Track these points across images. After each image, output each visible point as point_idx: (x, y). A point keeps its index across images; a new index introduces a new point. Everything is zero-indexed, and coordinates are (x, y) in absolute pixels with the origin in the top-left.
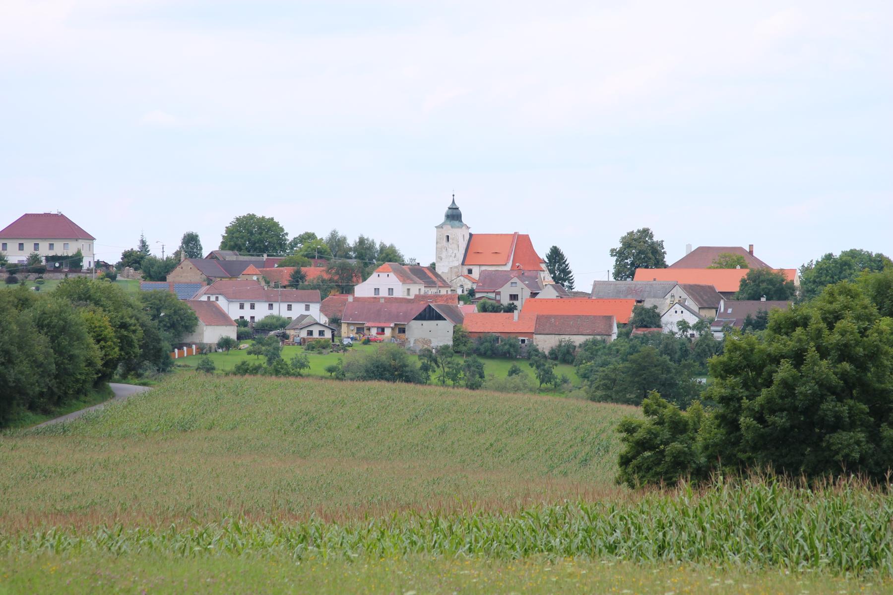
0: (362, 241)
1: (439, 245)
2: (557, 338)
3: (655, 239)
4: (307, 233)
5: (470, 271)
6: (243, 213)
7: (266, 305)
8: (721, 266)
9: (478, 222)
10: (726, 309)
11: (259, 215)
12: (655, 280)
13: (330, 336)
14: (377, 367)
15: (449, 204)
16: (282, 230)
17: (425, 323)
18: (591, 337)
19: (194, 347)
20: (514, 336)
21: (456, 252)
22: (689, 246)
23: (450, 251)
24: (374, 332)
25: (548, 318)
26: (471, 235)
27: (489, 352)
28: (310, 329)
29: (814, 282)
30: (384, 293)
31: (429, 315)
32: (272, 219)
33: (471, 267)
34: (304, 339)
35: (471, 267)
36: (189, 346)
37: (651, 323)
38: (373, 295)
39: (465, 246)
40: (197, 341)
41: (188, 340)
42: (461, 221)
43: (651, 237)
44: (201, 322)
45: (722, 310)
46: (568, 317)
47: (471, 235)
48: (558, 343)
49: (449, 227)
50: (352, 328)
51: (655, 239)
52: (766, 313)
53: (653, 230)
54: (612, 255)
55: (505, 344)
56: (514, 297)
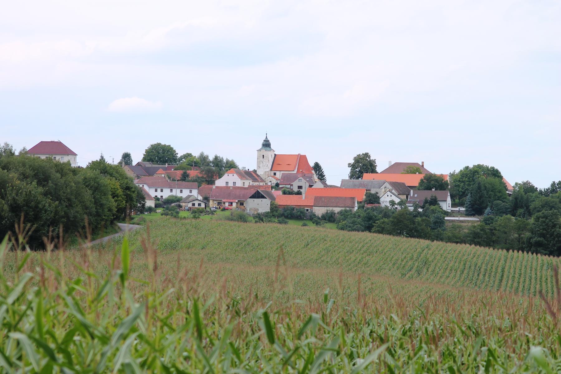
2: (326, 208)
3: (371, 158)
5: (275, 174)
6: (155, 142)
7: (169, 190)
9: (279, 148)
10: (414, 195)
11: (163, 143)
13: (204, 206)
15: (264, 138)
16: (175, 151)
17: (255, 200)
18: (344, 208)
22: (390, 162)
23: (265, 163)
24: (227, 204)
25: (321, 198)
26: (275, 155)
28: (193, 202)
29: (459, 181)
31: (257, 195)
38: (225, 185)
39: (272, 161)
43: (369, 157)
50: (215, 202)
51: (371, 158)
52: (435, 197)
56: (300, 187)
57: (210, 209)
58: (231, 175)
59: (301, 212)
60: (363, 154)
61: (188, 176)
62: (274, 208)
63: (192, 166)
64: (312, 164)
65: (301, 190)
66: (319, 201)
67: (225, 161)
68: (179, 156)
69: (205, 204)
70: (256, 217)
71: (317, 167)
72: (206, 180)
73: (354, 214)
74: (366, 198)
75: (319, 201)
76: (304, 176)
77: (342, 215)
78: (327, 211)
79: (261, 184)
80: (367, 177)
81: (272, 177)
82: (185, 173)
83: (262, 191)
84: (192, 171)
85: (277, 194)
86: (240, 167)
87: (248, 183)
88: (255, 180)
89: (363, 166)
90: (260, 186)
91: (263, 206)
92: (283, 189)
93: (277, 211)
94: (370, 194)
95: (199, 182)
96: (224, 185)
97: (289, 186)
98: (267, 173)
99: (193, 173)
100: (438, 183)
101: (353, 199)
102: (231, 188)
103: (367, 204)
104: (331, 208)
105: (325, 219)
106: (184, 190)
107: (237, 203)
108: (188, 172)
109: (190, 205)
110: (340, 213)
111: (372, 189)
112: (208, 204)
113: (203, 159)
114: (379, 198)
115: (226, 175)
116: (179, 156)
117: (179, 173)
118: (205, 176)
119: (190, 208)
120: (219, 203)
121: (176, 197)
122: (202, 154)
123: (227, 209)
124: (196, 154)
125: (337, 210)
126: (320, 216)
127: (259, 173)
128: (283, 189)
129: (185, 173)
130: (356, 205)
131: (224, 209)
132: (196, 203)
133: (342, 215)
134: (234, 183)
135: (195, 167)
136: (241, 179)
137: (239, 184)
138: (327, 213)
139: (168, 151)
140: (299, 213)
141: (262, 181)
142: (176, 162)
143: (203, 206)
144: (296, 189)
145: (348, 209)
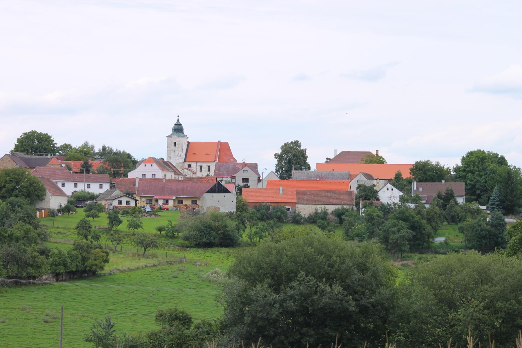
0: (104, 148)
1: (169, 149)
2: (314, 206)
3: (302, 148)
4: (65, 144)
5: (189, 166)
6: (28, 130)
7: (73, 184)
8: (367, 162)
9: (193, 134)
10: (417, 188)
11: (39, 131)
12: (333, 170)
13: (134, 205)
14: (206, 227)
15: (175, 122)
16: (53, 141)
17: (215, 195)
18: (340, 207)
19: (43, 211)
20: (282, 205)
21: (181, 153)
22: (336, 151)
23: (177, 152)
24: (160, 202)
25: (305, 192)
26: (189, 143)
27: (265, 217)
28: (120, 199)
29: (464, 171)
30: (149, 176)
31: (218, 189)
32: (47, 134)
33: (190, 163)
34: (116, 207)
35: (190, 163)
36: (40, 210)
37: (373, 197)
38: (151, 178)
39: (185, 149)
40: (46, 207)
41: (38, 206)
42: (183, 133)
43: (300, 146)
44: (48, 193)
45: (415, 189)
46: (320, 191)
47: (189, 143)
48: (314, 211)
49: (176, 137)
50: (144, 199)
51: (302, 148)
52: (452, 191)
53: (301, 141)
54: (275, 158)
55: (277, 211)
56: (245, 180)
60: (292, 142)
75: (303, 197)
89: (292, 159)
100: (437, 173)
104: (323, 207)
139: (46, 140)
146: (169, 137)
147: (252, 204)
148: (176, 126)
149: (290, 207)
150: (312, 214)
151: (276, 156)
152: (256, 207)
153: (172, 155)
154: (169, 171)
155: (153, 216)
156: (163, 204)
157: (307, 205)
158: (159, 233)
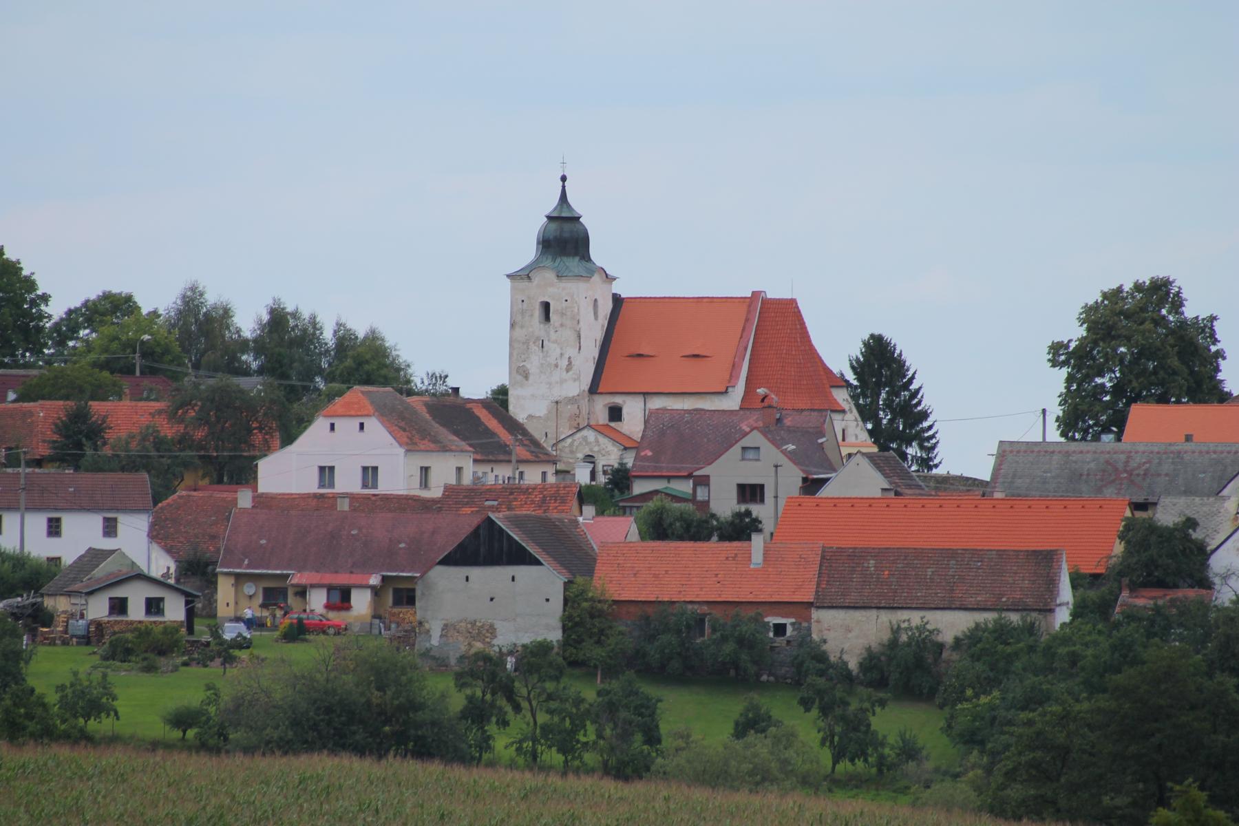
1: (519, 332)
2: (886, 617)
3: (1189, 312)
4: (107, 296)
5: (615, 413)
9: (641, 259)
12: (1188, 438)
14: (329, 710)
15: (550, 204)
16: (30, 284)
17: (476, 572)
18: (990, 616)
21: (571, 352)
23: (553, 350)
24: (317, 601)
25: (856, 556)
26: (617, 300)
28: (119, 593)
30: (348, 482)
31: (487, 547)
33: (618, 400)
35: (618, 400)
39: (599, 334)
43: (1178, 304)
46: (920, 553)
48: (886, 636)
49: (550, 275)
50: (249, 589)
51: (1189, 312)
54: (1055, 363)
55: (724, 639)
56: (750, 493)
57: (215, 632)
58: (347, 426)
59: (741, 642)
60: (1138, 287)
61: (95, 433)
62: (584, 618)
63: (128, 370)
64: (839, 352)
65: (756, 510)
66: (848, 576)
67: (328, 336)
68: (56, 310)
69: (190, 600)
70: (473, 674)
71: (881, 365)
72: (206, 459)
73: (1049, 651)
74: (1128, 552)
76: (775, 429)
77: (976, 658)
78: (896, 631)
79: (532, 476)
80: (1153, 426)
81: (599, 429)
82: (79, 417)
83: (517, 522)
84: (126, 402)
85: (611, 533)
86: (419, 377)
87: (450, 468)
88: (490, 451)
90: (510, 493)
91: (519, 608)
92: (651, 505)
93: (600, 637)
94: (1153, 528)
95: (156, 473)
96: (309, 484)
97: (685, 487)
98: (570, 409)
99: (129, 416)
101: (1046, 560)
102: (344, 505)
103: (1134, 588)
104: (915, 618)
105: (881, 683)
106: (70, 522)
107: (377, 592)
108: (97, 408)
109: (98, 609)
110: (970, 641)
111: (1165, 501)
112: (211, 602)
113: (200, 326)
114: (1202, 553)
115: (320, 425)
116: (56, 310)
117: (47, 414)
118: (199, 434)
119: (99, 625)
120: (274, 596)
121: (19, 561)
122: (191, 303)
123: (321, 628)
124: (157, 297)
125: (951, 625)
126: (853, 665)
127: (519, 409)
128: (651, 505)
129: (79, 417)
130: (1066, 593)
131: (298, 632)
132: (137, 597)
133: (976, 658)
134: (370, 474)
135: (146, 382)
136: (411, 447)
137: (399, 476)
138: (893, 644)
140: (729, 647)
141: (538, 454)
142: (37, 351)
143: (175, 611)
144: (725, 505)
145: (1015, 618)
146: (521, 276)
147: (632, 609)
148: (553, 226)
149: (788, 621)
150: (874, 645)
151: (1058, 355)
152: (647, 618)
153: (534, 363)
154: (445, 449)
155: (218, 661)
156: (329, 606)
157: (858, 615)
158: (177, 734)
